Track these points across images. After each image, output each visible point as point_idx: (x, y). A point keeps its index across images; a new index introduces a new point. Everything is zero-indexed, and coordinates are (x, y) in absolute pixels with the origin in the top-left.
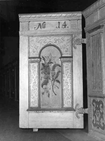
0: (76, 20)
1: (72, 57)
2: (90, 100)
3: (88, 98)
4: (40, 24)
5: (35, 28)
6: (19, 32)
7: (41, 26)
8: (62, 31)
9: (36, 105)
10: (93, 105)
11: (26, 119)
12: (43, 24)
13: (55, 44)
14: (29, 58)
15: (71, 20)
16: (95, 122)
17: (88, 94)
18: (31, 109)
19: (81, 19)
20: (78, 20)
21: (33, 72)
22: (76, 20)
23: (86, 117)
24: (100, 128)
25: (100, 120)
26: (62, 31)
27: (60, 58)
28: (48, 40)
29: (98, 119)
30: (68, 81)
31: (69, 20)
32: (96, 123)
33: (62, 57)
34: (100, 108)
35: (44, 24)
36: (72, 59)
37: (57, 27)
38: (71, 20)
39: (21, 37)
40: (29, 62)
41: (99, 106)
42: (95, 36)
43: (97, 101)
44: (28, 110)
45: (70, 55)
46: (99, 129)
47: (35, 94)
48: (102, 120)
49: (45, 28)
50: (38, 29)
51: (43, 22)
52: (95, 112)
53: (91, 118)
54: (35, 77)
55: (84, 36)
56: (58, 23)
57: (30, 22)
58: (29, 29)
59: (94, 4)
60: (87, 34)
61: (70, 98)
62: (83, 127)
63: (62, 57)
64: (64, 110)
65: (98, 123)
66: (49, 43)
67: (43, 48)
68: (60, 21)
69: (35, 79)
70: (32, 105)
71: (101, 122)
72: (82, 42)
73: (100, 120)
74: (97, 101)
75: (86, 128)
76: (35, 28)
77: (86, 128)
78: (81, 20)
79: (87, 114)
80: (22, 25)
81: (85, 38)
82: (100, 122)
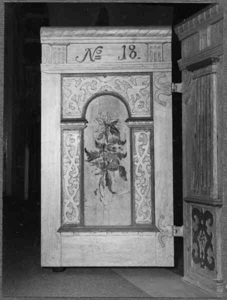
0: (63, 44)
1: (151, 119)
2: (187, 210)
3: (185, 204)
4: (89, 50)
5: (77, 57)
6: (41, 65)
7: (92, 55)
8: (129, 64)
9: (76, 220)
10: (194, 219)
11: (58, 248)
12: (98, 48)
13: (117, 92)
14: (63, 121)
15: (54, 44)
16: (196, 254)
17: (185, 194)
18: (65, 228)
19: (170, 41)
20: (67, 46)
21: (69, 151)
22: (63, 44)
23: (179, 242)
24: (205, 267)
25: (206, 251)
26: (129, 64)
27: (127, 121)
28: (103, 84)
29: (202, 249)
30: (144, 169)
31: (146, 43)
32: (199, 256)
33: (130, 119)
34: (206, 227)
35: (98, 49)
36: (152, 122)
37: (119, 57)
38: (54, 44)
39: (43, 75)
40: (63, 130)
41: (205, 222)
42: (205, 77)
43: (202, 211)
44: (61, 230)
45: (149, 116)
46: (204, 268)
47: (73, 196)
48: (211, 250)
49: (99, 59)
50: (86, 60)
51: (99, 45)
52: (196, 234)
53: (189, 244)
54: (73, 160)
55: (177, 77)
56: (123, 48)
57: (69, 44)
58: (67, 62)
59: (194, 17)
60: (185, 75)
61: (149, 205)
62: (173, 265)
63: (130, 119)
64: (136, 229)
65: (202, 256)
66: (103, 90)
67: (97, 95)
68: (125, 44)
69: (73, 165)
70: (67, 221)
71: (207, 255)
72: (175, 235)
73: (206, 251)
74: (201, 211)
75: (178, 268)
76: (77, 57)
77: (178, 268)
78: (171, 73)
79: (182, 238)
80: (47, 52)
81: (181, 82)
82: (206, 255)
